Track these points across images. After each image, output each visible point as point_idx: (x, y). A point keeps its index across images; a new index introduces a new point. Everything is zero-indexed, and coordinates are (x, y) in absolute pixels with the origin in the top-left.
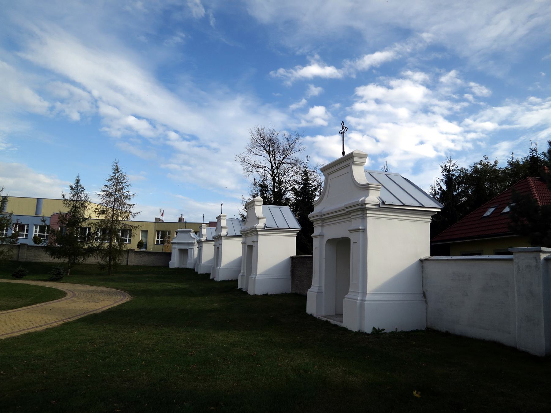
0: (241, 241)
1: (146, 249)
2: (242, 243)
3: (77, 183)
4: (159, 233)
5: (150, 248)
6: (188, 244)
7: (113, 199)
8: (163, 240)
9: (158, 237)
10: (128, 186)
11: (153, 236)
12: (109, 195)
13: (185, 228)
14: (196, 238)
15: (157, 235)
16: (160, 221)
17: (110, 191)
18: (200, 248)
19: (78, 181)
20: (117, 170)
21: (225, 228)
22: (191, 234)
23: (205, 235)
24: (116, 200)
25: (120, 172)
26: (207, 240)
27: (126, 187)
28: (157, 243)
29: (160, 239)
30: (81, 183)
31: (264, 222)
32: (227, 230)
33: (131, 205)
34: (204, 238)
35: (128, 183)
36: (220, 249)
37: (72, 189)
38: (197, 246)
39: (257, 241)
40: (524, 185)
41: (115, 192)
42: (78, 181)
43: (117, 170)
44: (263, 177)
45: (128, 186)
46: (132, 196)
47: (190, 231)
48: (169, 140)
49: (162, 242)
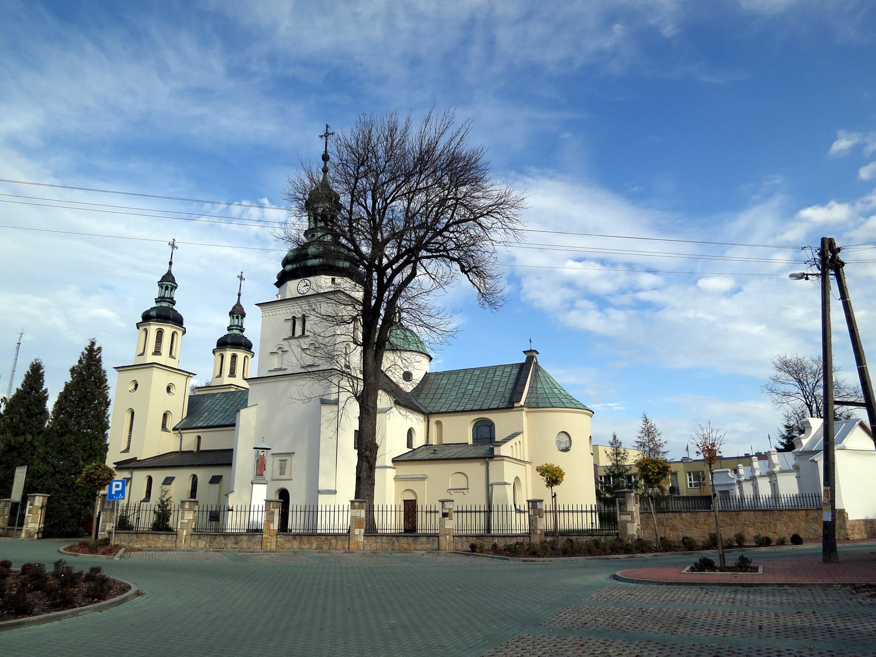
0: (795, 476)
1: (679, 494)
2: (796, 477)
3: (615, 439)
4: (690, 475)
5: (683, 492)
6: (728, 485)
7: (647, 449)
8: (611, 477)
9: (690, 480)
10: (658, 435)
11: (684, 479)
12: (642, 445)
13: (721, 468)
14: (735, 478)
15: (688, 477)
16: (689, 461)
17: (644, 441)
18: (755, 485)
19: (615, 437)
20: (646, 421)
21: (757, 469)
22: (729, 474)
23: (743, 475)
24: (650, 450)
25: (650, 423)
26: (746, 480)
27: (658, 436)
28: (690, 486)
29: (693, 482)
30: (617, 438)
31: (780, 466)
32: (759, 471)
33: (665, 453)
34: (743, 478)
35: (659, 432)
36: (776, 485)
37: (612, 444)
38: (738, 487)
39: (777, 481)
40: (675, 503)
41: (648, 442)
42: (615, 437)
43: (646, 421)
44: (787, 418)
45: (658, 435)
46: (664, 444)
47: (728, 471)
48: (640, 290)
49: (696, 485)
